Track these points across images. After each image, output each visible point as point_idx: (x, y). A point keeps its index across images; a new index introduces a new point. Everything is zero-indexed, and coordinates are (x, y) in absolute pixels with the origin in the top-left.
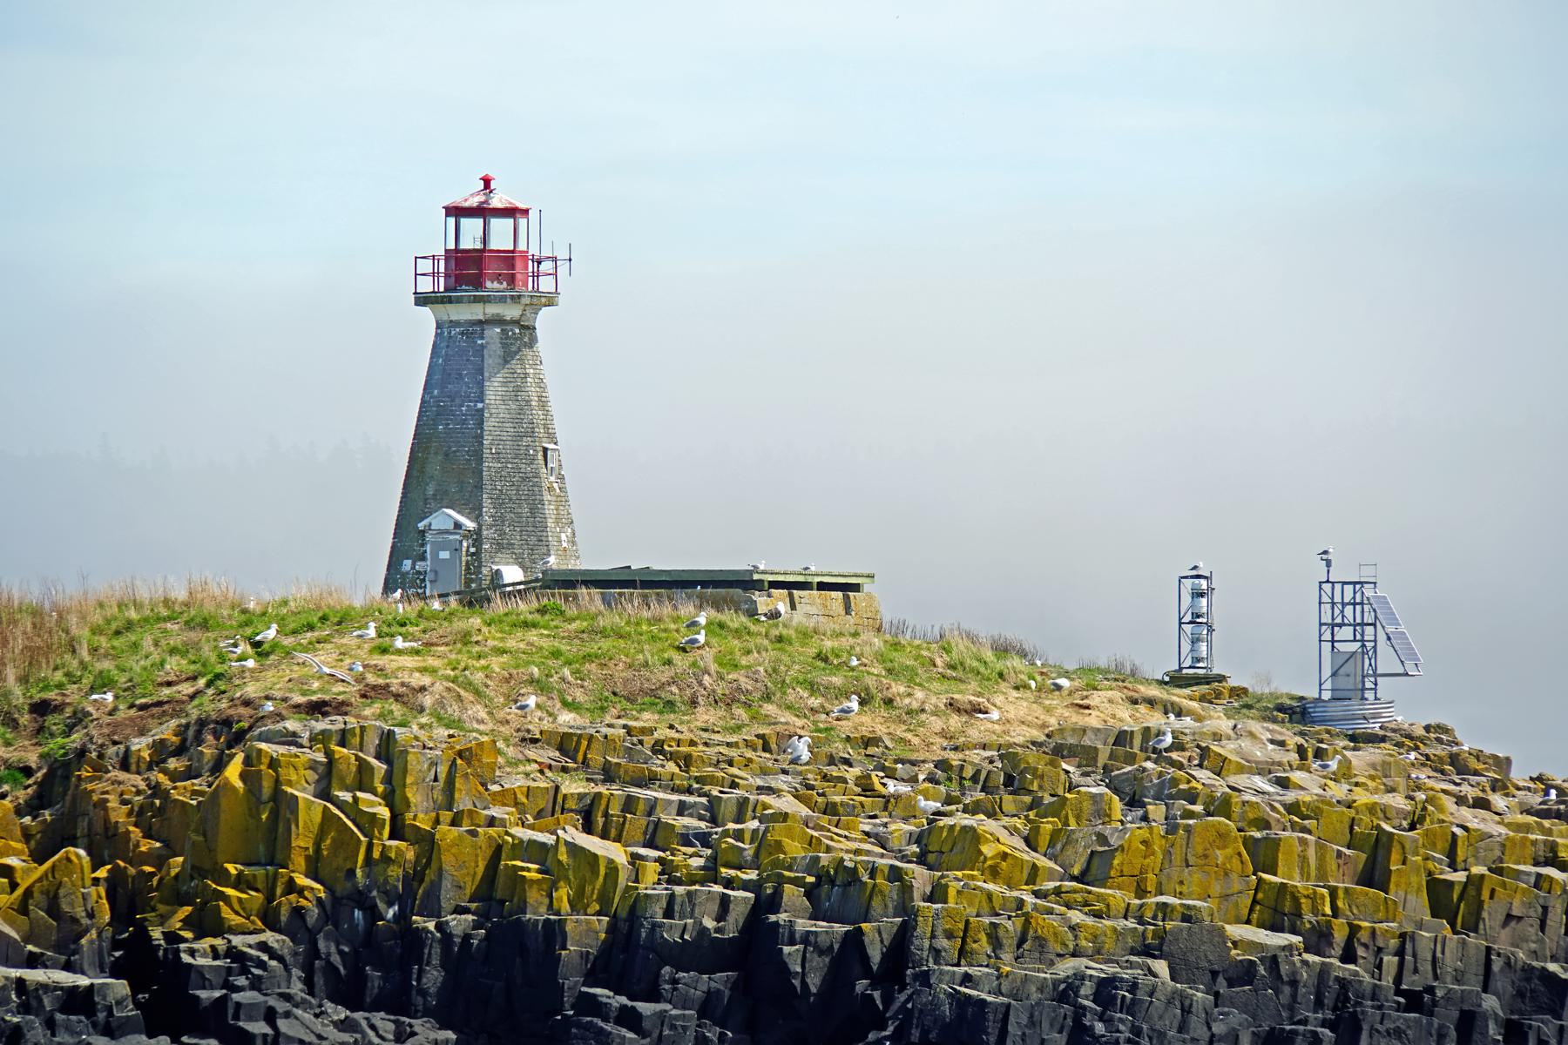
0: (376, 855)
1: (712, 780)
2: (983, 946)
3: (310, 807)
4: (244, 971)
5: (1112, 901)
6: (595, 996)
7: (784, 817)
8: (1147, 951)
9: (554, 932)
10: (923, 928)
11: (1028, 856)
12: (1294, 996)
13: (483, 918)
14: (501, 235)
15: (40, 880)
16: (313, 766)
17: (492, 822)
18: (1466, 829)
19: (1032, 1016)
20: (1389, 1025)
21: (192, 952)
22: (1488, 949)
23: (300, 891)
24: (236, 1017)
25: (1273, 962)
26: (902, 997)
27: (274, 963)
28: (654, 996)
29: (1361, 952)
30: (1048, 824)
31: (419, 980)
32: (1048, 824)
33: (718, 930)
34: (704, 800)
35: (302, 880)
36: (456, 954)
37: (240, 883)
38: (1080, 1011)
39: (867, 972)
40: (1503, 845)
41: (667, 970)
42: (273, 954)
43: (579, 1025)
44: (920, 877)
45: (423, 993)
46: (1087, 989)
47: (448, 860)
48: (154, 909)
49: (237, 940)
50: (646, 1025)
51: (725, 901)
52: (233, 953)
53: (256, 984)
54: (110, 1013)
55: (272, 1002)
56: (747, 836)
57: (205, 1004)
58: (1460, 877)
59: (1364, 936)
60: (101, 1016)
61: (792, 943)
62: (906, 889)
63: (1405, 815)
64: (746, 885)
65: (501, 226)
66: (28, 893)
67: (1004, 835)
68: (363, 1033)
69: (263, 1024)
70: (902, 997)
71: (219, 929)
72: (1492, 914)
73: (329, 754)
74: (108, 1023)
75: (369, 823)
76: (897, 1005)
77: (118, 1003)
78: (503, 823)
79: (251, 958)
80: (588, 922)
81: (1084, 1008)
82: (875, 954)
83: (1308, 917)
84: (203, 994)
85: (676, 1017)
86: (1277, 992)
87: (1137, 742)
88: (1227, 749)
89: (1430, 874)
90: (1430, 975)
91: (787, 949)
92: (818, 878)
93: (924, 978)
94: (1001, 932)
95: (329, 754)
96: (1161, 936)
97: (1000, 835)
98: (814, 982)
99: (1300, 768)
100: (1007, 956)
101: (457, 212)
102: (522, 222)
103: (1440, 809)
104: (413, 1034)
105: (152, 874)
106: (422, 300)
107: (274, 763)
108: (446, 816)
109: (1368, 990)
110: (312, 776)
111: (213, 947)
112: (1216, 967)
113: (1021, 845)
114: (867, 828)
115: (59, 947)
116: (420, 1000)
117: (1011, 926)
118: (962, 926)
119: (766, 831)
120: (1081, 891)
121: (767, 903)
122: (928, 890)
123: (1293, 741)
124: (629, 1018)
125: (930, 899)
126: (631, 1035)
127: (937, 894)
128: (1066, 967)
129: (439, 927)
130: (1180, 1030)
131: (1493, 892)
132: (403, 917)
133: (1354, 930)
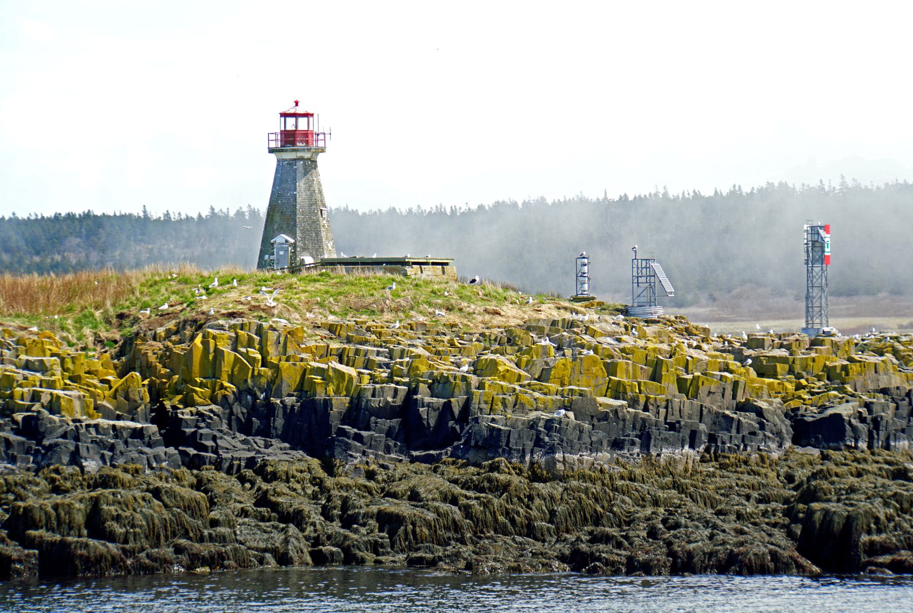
0: (256, 373)
2: (500, 407)
3: (229, 355)
4: (204, 421)
7: (419, 356)
9: (327, 403)
10: (475, 400)
11: (517, 371)
12: (624, 425)
13: (299, 398)
14: (303, 124)
16: (230, 338)
17: (302, 360)
20: (662, 436)
21: (183, 414)
23: (226, 388)
24: (201, 439)
25: (616, 412)
29: (651, 407)
30: (525, 358)
32: (525, 358)
33: (393, 402)
35: (226, 384)
36: (289, 413)
37: (201, 385)
38: (539, 432)
39: (453, 418)
42: (215, 414)
43: (338, 441)
46: (541, 424)
49: (201, 408)
51: (396, 390)
52: (200, 414)
53: (208, 426)
57: (188, 434)
58: (690, 377)
59: (652, 401)
63: (667, 352)
64: (404, 384)
65: (302, 122)
67: (507, 363)
70: (467, 428)
71: (193, 404)
72: (703, 391)
73: (236, 333)
75: (252, 361)
76: (465, 431)
78: (306, 360)
79: (206, 415)
82: (456, 411)
83: (630, 394)
87: (560, 324)
88: (596, 327)
91: (421, 409)
92: (433, 380)
93: (476, 420)
95: (236, 333)
97: (506, 362)
99: (626, 334)
101: (285, 115)
102: (311, 119)
103: (682, 350)
106: (271, 151)
107: (214, 338)
108: (284, 358)
110: (230, 342)
115: (129, 412)
117: (510, 399)
121: (413, 391)
125: (478, 388)
127: (481, 386)
128: (533, 415)
129: (281, 402)
132: (267, 398)
133: (648, 398)
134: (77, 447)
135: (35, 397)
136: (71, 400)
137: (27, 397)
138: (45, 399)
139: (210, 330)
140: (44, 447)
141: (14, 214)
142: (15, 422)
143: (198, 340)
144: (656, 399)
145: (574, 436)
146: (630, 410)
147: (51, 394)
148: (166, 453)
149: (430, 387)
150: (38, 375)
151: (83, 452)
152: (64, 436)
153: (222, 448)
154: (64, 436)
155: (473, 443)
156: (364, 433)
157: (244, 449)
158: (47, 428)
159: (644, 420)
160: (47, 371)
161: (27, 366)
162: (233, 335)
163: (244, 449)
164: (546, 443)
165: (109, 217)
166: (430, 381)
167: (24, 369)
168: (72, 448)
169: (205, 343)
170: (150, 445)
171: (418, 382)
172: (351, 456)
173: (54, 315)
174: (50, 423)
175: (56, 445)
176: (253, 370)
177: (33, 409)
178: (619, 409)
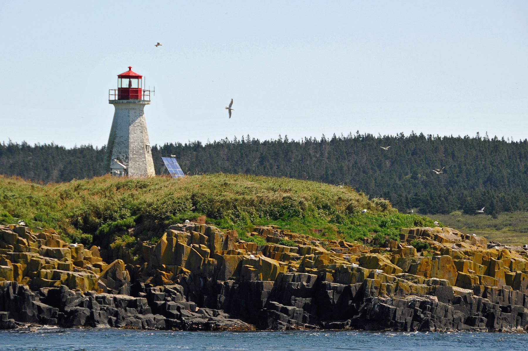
0: (206, 262)
1: (299, 242)
2: (385, 291)
4: (170, 296)
5: (420, 279)
6: (274, 304)
7: (322, 253)
8: (430, 294)
9: (260, 286)
10: (369, 285)
11: (393, 266)
12: (471, 308)
13: (237, 281)
14: (135, 84)
15: (110, 269)
16: (187, 237)
17: (239, 253)
18: (515, 260)
19: (402, 312)
20: (502, 316)
21: (154, 290)
22: (524, 295)
23: (184, 273)
24: (169, 309)
25: (465, 297)
26: (363, 306)
27: (178, 293)
28: (290, 305)
29: (488, 295)
30: (397, 256)
31: (219, 299)
32: (397, 256)
33: (307, 286)
34: (297, 248)
35: (184, 269)
36: (230, 292)
37: (167, 270)
38: (416, 311)
39: (352, 298)
40: (525, 265)
41: (293, 297)
42: (178, 291)
43: (270, 312)
44: (366, 271)
45: (220, 302)
46: (418, 304)
47: (227, 264)
48: (141, 277)
49: (167, 287)
50: (290, 313)
51: (309, 277)
52: (166, 291)
53: (173, 299)
54: (142, 308)
55: (179, 305)
56: (313, 259)
57: (159, 305)
58: (514, 274)
59: (489, 290)
60: (139, 308)
61: (330, 290)
62: (362, 274)
63: (496, 255)
64: (314, 273)
66: (107, 272)
67: (385, 259)
68: (204, 314)
69: (176, 311)
70: (363, 306)
71: (161, 283)
73: (192, 233)
74: (141, 310)
75: (204, 253)
76: (361, 308)
77: (144, 305)
78: (242, 254)
79: (172, 292)
80: (269, 283)
81: (417, 310)
82: (354, 293)
83: (473, 285)
84: (158, 302)
85: (298, 311)
86: (466, 306)
87: (415, 232)
88: (442, 235)
89: (505, 272)
90: (508, 302)
91: (329, 291)
92: (336, 271)
93: (370, 300)
94: (391, 288)
95: (192, 233)
96: (434, 289)
98: (336, 301)
99: (463, 241)
100: (392, 295)
101: (121, 77)
102: (140, 80)
103: (506, 254)
104: (219, 314)
105: (139, 267)
106: (111, 102)
107: (176, 236)
108: (226, 252)
109: (492, 306)
110: (187, 240)
111: (160, 289)
112: (450, 299)
113: (389, 262)
114: (344, 257)
115: (116, 288)
116: (220, 305)
117: (393, 285)
118: (379, 285)
119: (318, 257)
120: (410, 276)
121: (321, 278)
122: (368, 275)
123: (460, 233)
124: (285, 311)
125: (369, 277)
126: (285, 315)
127: (371, 276)
128: (411, 298)
129: (225, 283)
130: (445, 317)
131: (524, 278)
132: (214, 281)
133: (486, 289)
134: (92, 313)
135: (56, 276)
136: (83, 279)
137: (50, 276)
138: (64, 277)
139: (173, 231)
140: (66, 312)
141: (227, 138)
142: (42, 294)
143: (165, 237)
144: (492, 289)
145: (442, 313)
146: (475, 296)
147: (68, 274)
148: (155, 318)
149: (334, 275)
150: (56, 260)
151: (96, 317)
152: (81, 304)
153: (184, 316)
154: (81, 304)
155: (368, 317)
156: (290, 308)
157: (199, 317)
158: (67, 299)
159: (484, 304)
160: (62, 257)
161: (48, 253)
162: (189, 234)
163: (199, 317)
164: (422, 319)
165: (315, 143)
166: (333, 271)
167: (44, 256)
168: (88, 314)
169: (170, 239)
170: (141, 312)
171: (325, 272)
172: (281, 324)
173: (364, 208)
174: (70, 295)
175: (76, 311)
176: (205, 260)
177: (56, 284)
178: (467, 295)
